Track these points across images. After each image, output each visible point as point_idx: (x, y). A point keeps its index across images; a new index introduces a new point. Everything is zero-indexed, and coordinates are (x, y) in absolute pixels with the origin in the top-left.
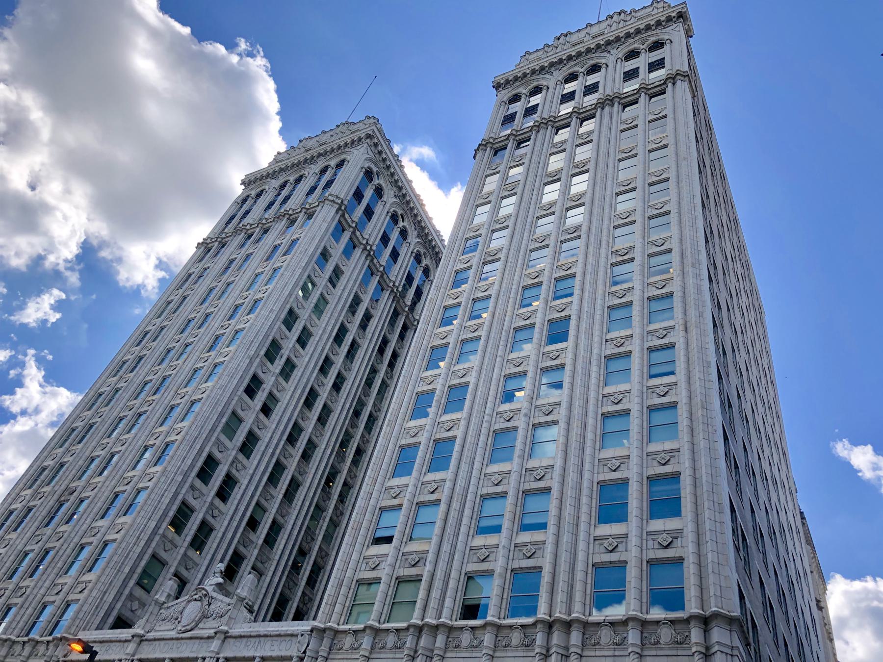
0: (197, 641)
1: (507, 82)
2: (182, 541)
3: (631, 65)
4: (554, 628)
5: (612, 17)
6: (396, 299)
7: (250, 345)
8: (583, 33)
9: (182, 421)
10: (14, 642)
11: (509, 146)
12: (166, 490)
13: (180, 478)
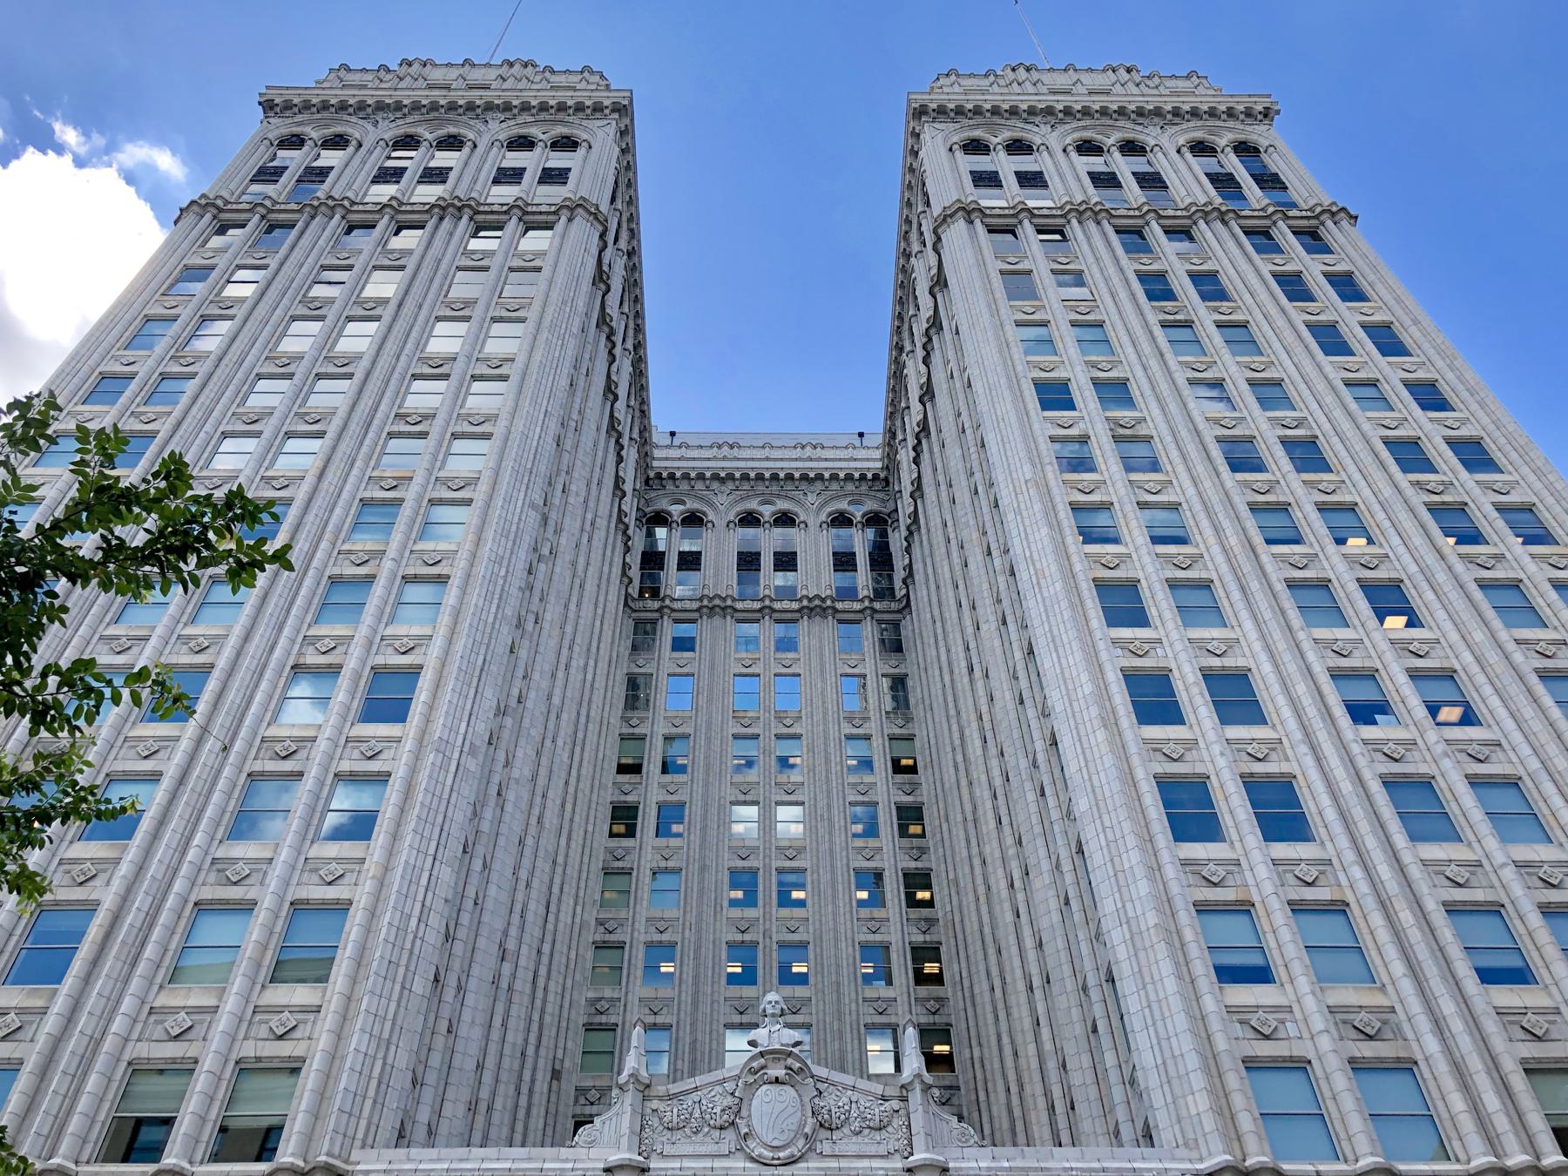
3: (514, 159)
8: (454, 73)
11: (250, 226)
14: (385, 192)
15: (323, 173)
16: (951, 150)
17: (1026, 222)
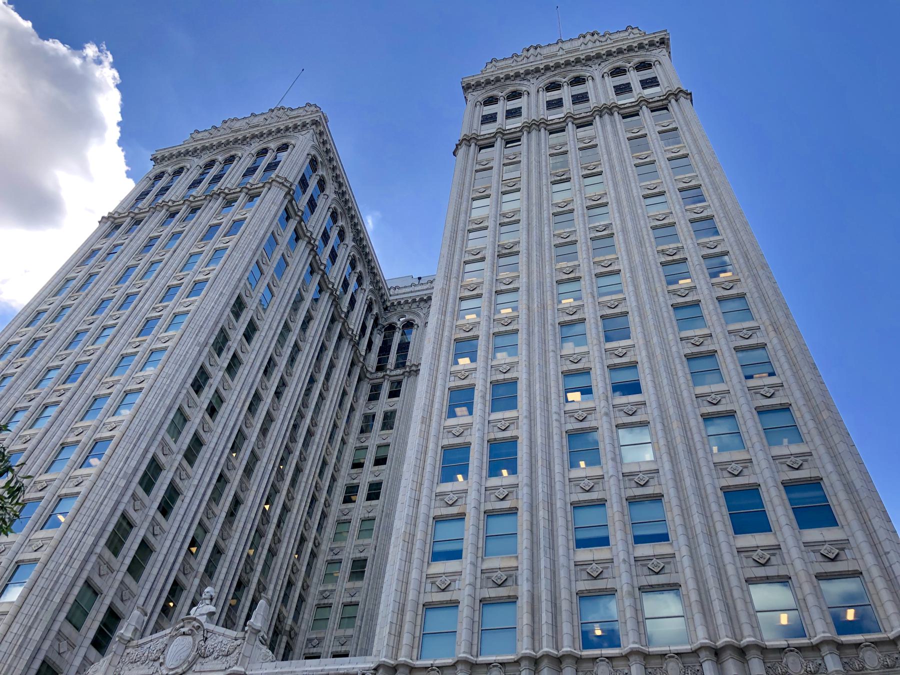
1: (171, 156)
2: (119, 564)
3: (489, 110)
5: (584, 37)
9: (81, 420)
12: (105, 497)
13: (122, 483)
14: (490, 129)
16: (603, 77)
17: (644, 108)
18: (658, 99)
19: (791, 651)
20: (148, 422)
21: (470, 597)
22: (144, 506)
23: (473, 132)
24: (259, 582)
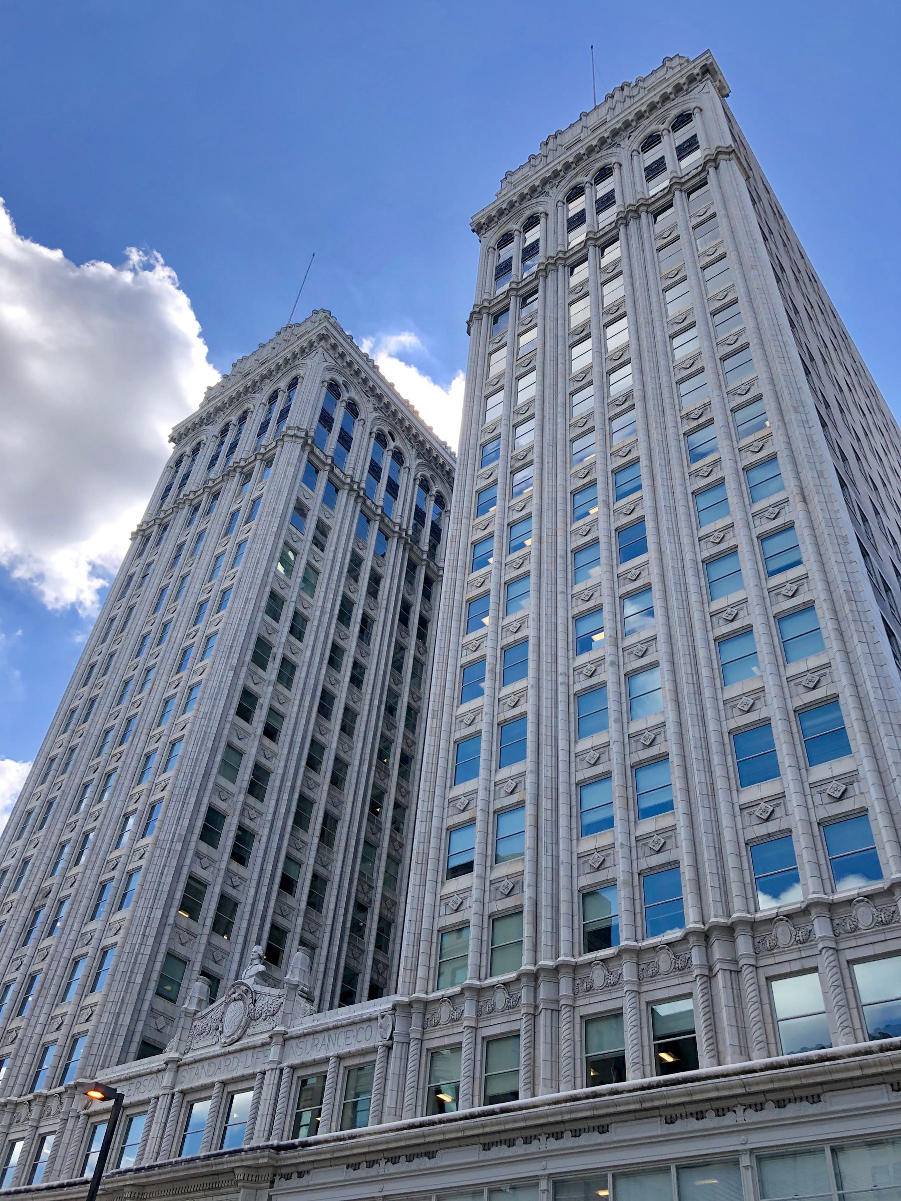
0: (250, 1052)
3: (576, 207)
4: (713, 939)
6: (408, 546)
7: (230, 652)
8: (577, 128)
10: (17, 1104)
12: (165, 866)
13: (179, 847)
14: (660, 184)
15: (535, 246)
18: (695, 172)
19: (781, 920)
20: (192, 773)
21: (476, 916)
22: (214, 861)
23: (638, 197)
24: (384, 897)
